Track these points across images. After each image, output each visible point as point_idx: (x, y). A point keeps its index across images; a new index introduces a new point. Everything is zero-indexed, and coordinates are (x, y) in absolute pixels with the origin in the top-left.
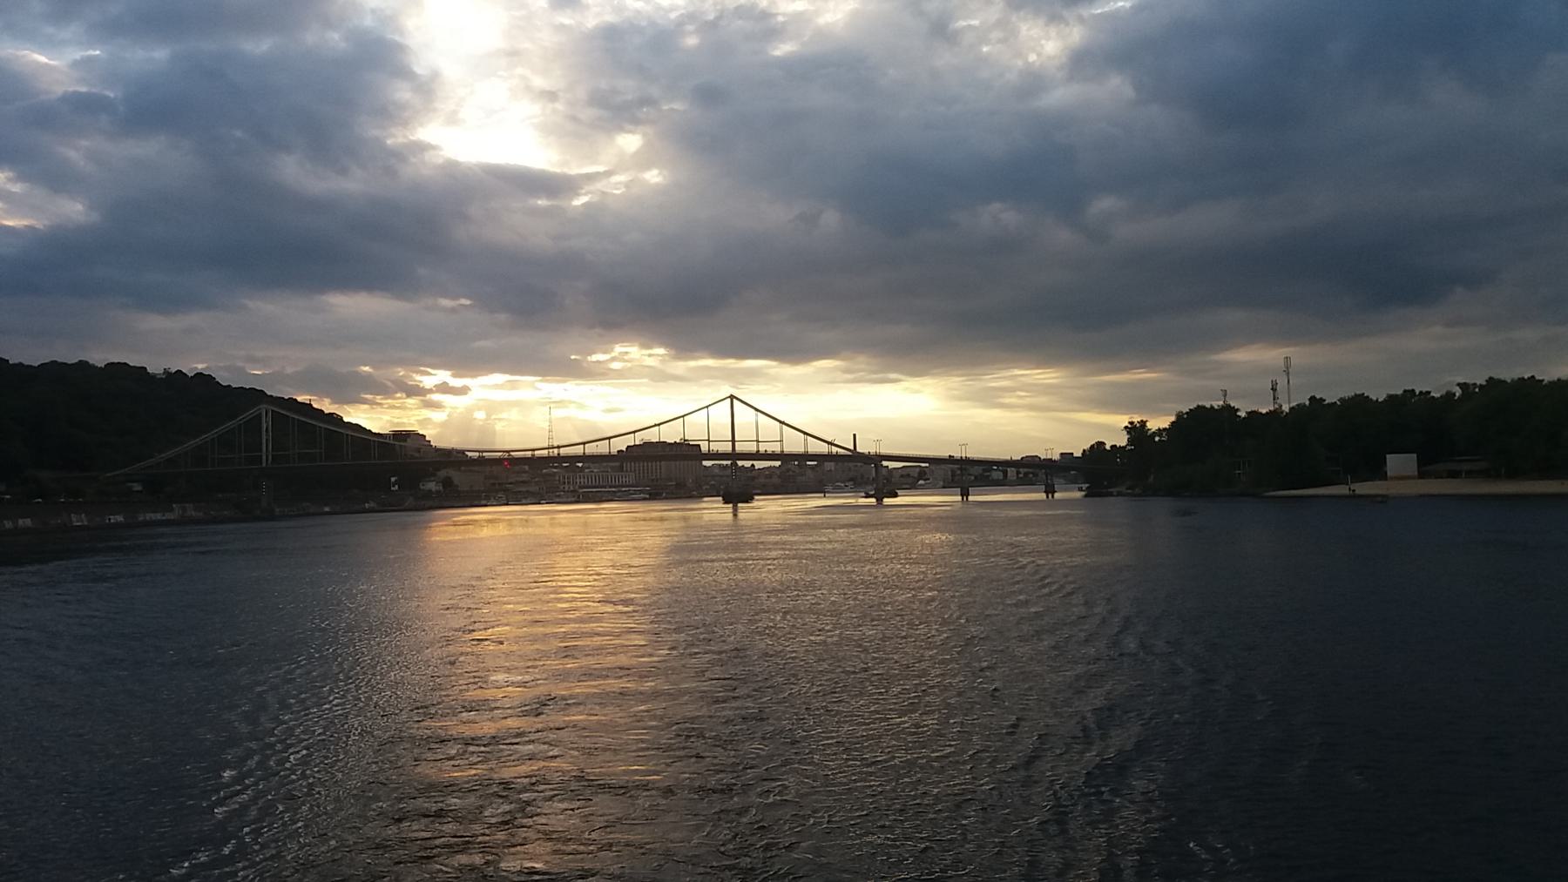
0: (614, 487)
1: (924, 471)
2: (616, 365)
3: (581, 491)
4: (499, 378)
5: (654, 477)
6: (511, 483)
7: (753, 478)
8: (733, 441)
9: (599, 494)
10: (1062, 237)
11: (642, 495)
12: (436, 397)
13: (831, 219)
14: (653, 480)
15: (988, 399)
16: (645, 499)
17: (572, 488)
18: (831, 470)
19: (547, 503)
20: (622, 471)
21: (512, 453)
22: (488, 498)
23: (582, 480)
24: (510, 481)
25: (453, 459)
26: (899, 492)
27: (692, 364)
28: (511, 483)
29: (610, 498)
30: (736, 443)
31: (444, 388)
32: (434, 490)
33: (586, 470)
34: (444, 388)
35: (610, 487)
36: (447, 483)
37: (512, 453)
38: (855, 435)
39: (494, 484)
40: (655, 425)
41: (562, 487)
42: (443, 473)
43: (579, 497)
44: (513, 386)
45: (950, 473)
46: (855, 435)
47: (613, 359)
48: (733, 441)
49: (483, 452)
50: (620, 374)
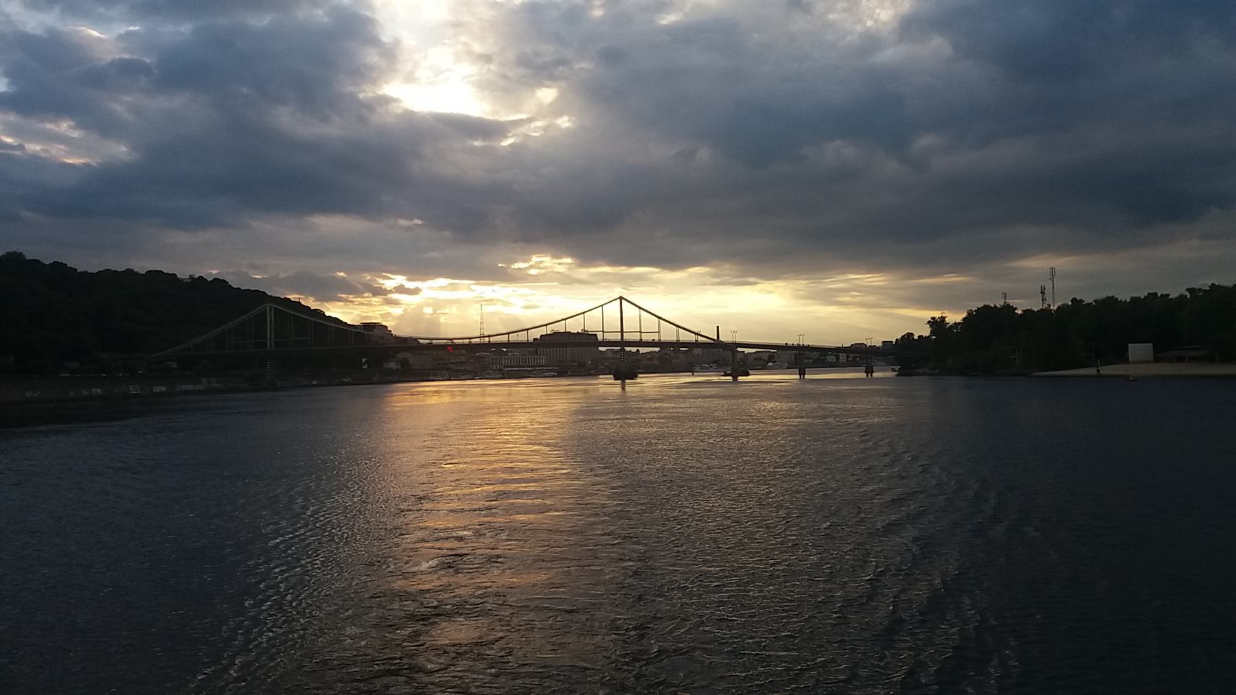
0: (530, 367)
1: (773, 355)
2: (533, 272)
3: (505, 369)
4: (442, 282)
5: (561, 359)
6: (453, 364)
7: (638, 360)
8: (622, 332)
9: (519, 372)
10: (891, 167)
11: (552, 373)
12: (395, 296)
13: (704, 154)
14: (560, 362)
15: (827, 298)
16: (554, 376)
17: (498, 368)
18: (699, 354)
19: (480, 379)
20: (537, 354)
21: (455, 341)
22: (435, 375)
23: (506, 361)
24: (452, 361)
25: (408, 344)
26: (751, 372)
27: (593, 270)
28: (453, 364)
29: (528, 375)
30: (624, 334)
31: (401, 289)
32: (394, 368)
33: (510, 354)
34: (401, 289)
35: (528, 367)
36: (404, 363)
37: (455, 341)
38: (718, 327)
39: (439, 364)
40: (563, 320)
41: (491, 367)
42: (401, 356)
43: (504, 374)
44: (454, 287)
45: (793, 357)
46: (718, 327)
47: (531, 267)
48: (622, 332)
49: (432, 339)
50: (536, 279)
